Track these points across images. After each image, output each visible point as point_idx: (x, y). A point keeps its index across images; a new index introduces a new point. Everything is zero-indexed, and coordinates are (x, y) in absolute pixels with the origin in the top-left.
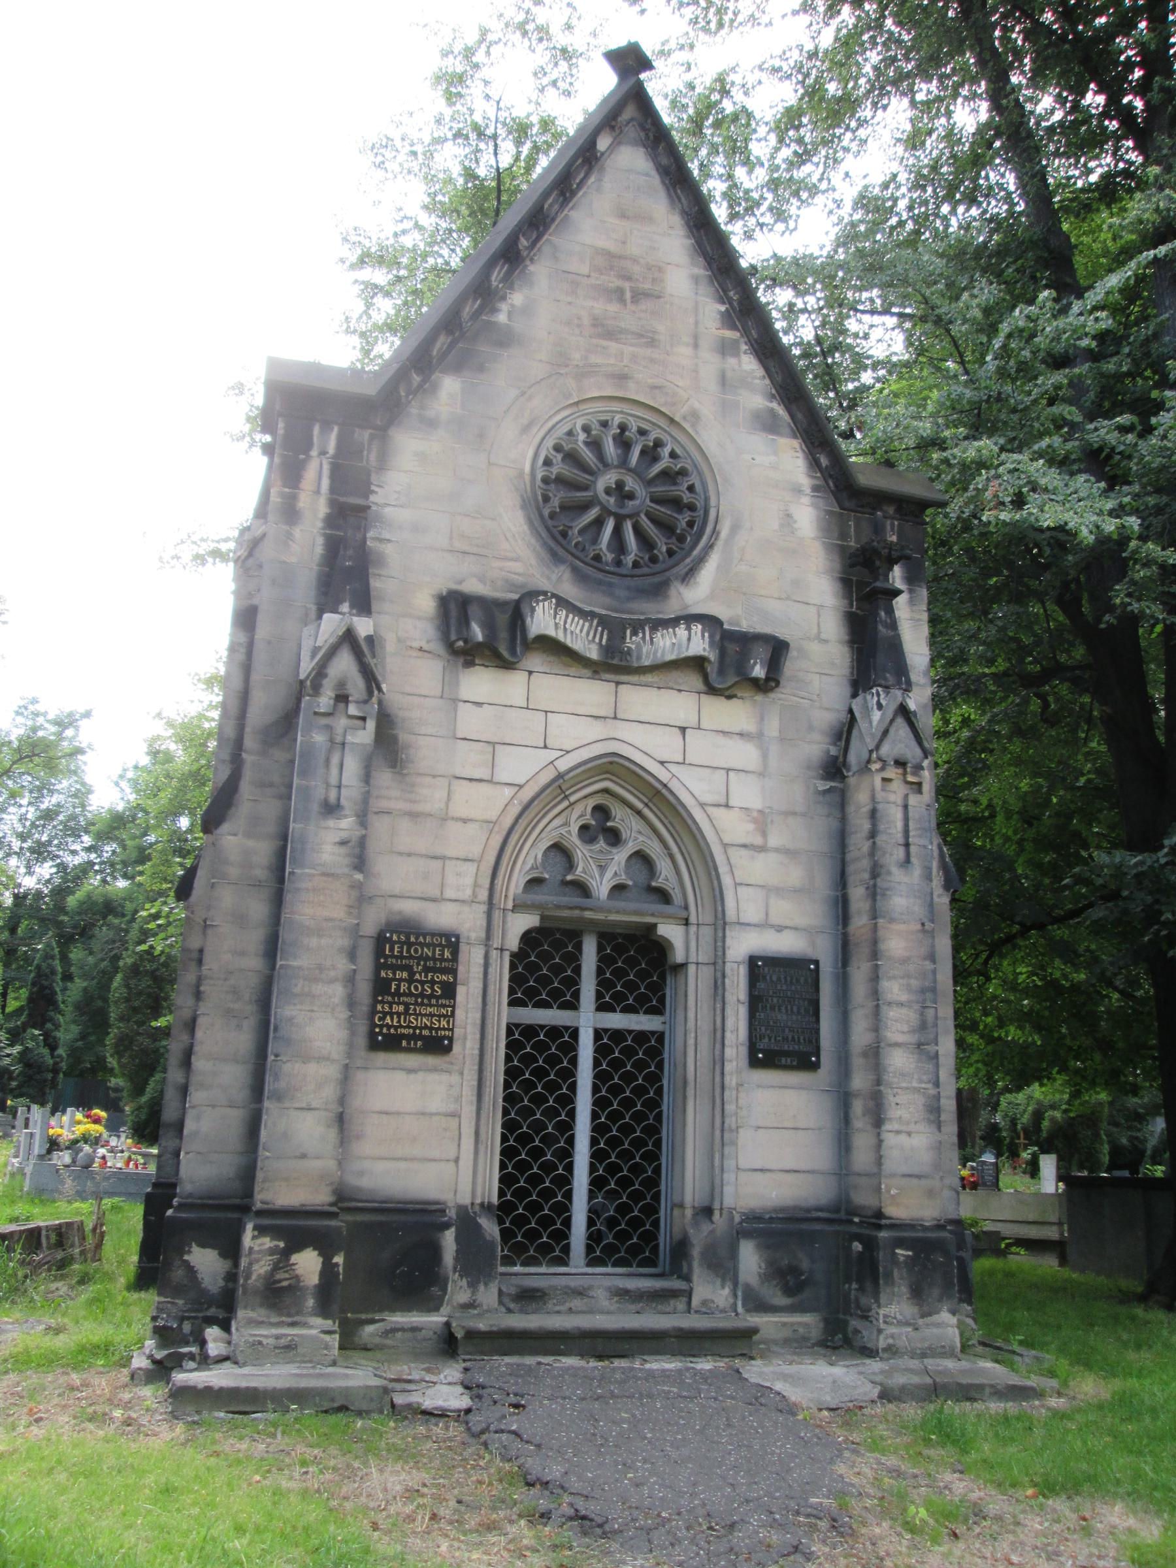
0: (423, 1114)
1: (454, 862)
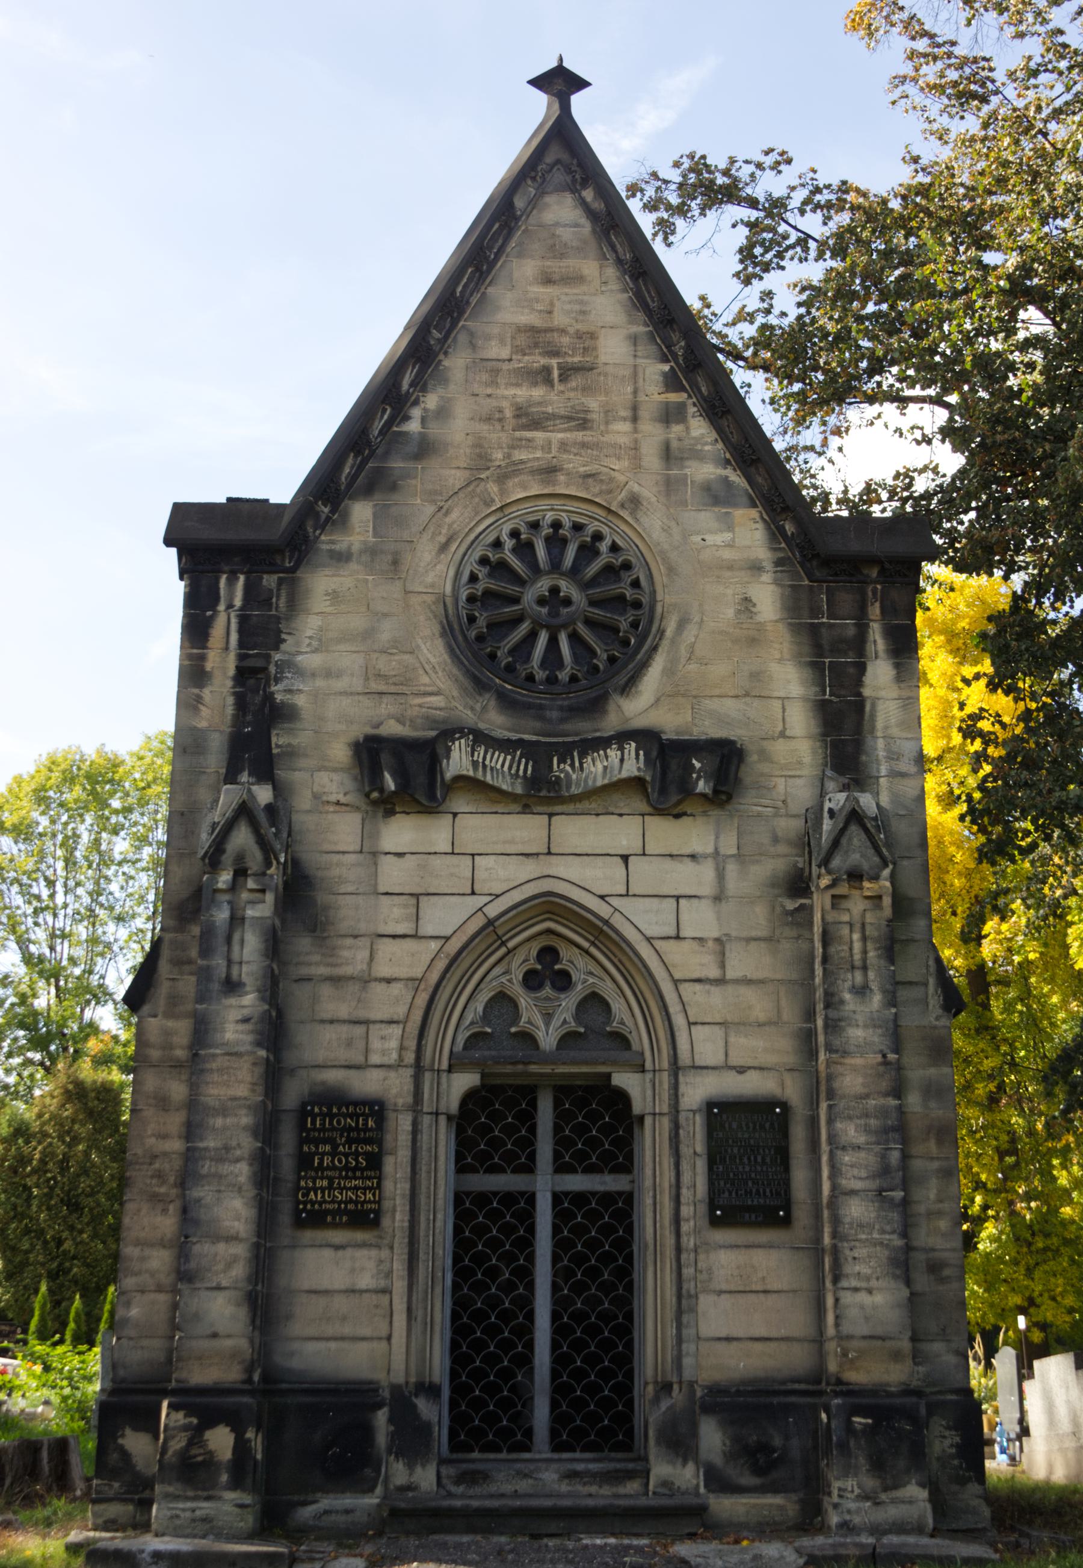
0: (353, 1291)
1: (378, 1026)
